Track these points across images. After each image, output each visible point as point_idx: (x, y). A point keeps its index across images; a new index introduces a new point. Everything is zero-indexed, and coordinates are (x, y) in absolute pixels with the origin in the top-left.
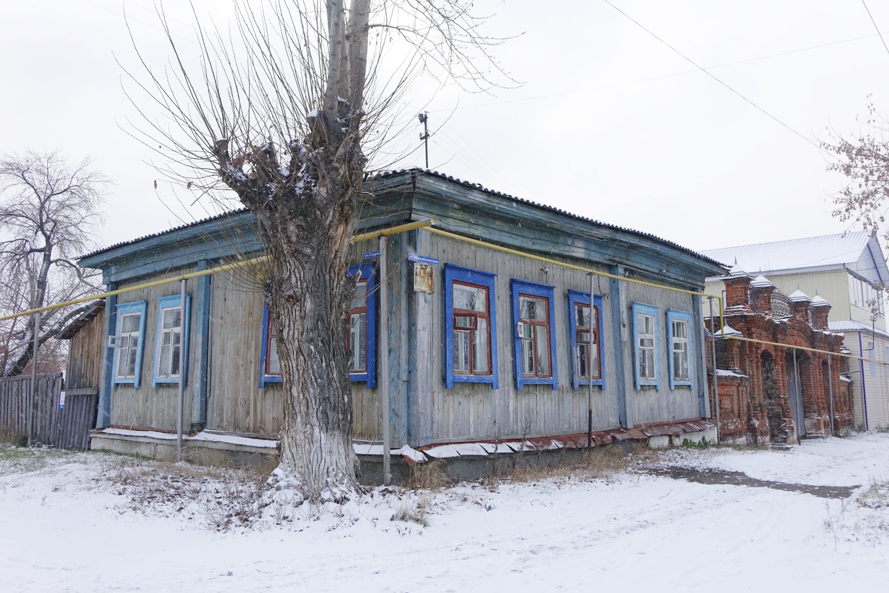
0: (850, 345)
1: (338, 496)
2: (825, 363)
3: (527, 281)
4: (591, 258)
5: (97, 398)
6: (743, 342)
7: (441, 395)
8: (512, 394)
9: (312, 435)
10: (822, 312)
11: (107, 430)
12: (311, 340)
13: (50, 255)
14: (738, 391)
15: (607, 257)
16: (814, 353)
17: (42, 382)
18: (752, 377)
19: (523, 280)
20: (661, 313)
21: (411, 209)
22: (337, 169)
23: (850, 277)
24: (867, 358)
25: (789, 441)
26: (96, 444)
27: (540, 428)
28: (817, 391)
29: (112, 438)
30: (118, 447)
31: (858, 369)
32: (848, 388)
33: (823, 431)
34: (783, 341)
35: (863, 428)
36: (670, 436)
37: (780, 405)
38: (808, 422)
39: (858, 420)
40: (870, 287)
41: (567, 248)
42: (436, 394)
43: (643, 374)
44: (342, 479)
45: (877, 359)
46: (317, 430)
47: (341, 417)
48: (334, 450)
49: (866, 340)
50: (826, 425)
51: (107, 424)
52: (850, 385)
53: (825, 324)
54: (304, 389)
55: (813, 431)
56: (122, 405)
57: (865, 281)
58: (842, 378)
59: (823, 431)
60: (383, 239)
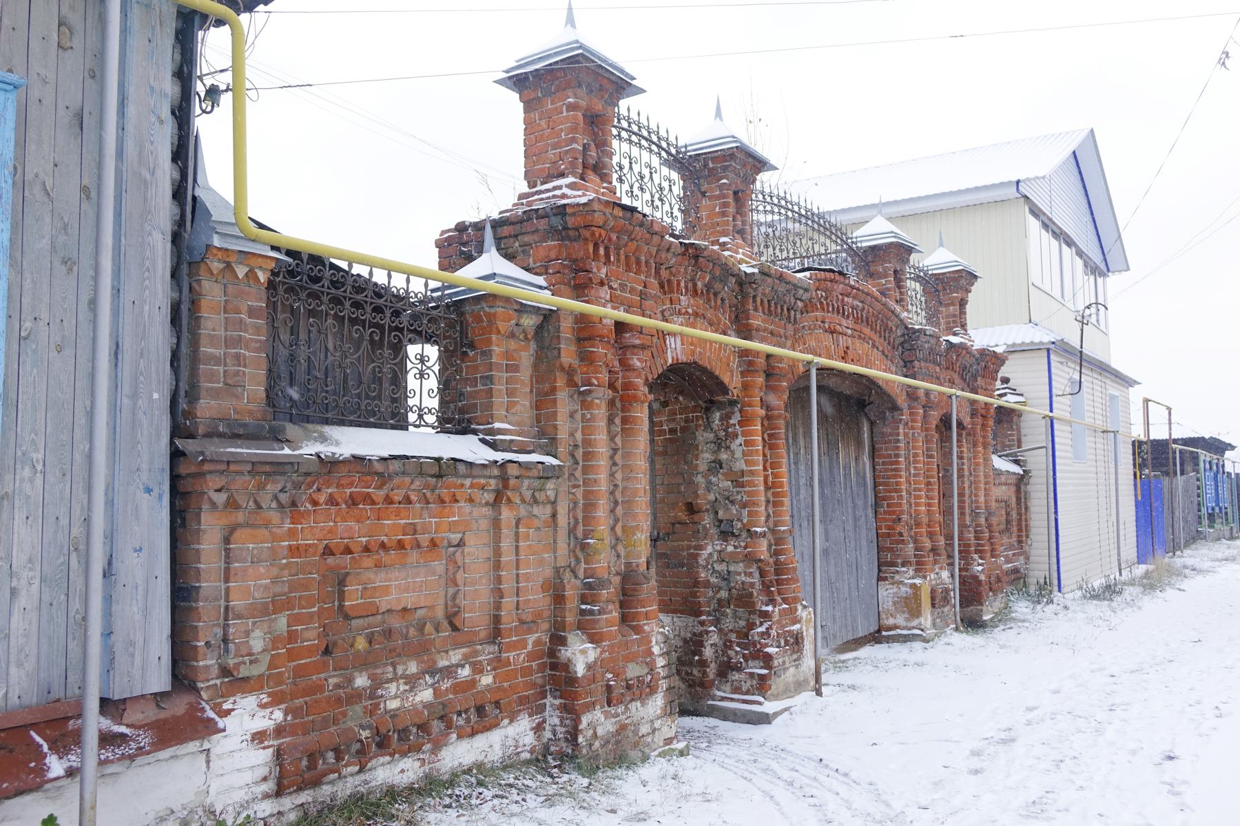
0: (1024, 384)
2: (945, 422)
6: (548, 317)
10: (951, 289)
14: (496, 524)
16: (912, 394)
18: (583, 456)
23: (1034, 224)
24: (1067, 416)
25: (776, 684)
28: (915, 498)
31: (1042, 439)
32: (1018, 491)
33: (926, 619)
34: (773, 337)
35: (1045, 592)
37: (750, 559)
38: (887, 593)
39: (1038, 570)
40: (1079, 263)
45: (1088, 420)
49: (1064, 373)
50: (938, 599)
52: (1021, 481)
53: (959, 322)
55: (900, 620)
57: (1070, 243)
58: (1000, 463)
59: (926, 619)
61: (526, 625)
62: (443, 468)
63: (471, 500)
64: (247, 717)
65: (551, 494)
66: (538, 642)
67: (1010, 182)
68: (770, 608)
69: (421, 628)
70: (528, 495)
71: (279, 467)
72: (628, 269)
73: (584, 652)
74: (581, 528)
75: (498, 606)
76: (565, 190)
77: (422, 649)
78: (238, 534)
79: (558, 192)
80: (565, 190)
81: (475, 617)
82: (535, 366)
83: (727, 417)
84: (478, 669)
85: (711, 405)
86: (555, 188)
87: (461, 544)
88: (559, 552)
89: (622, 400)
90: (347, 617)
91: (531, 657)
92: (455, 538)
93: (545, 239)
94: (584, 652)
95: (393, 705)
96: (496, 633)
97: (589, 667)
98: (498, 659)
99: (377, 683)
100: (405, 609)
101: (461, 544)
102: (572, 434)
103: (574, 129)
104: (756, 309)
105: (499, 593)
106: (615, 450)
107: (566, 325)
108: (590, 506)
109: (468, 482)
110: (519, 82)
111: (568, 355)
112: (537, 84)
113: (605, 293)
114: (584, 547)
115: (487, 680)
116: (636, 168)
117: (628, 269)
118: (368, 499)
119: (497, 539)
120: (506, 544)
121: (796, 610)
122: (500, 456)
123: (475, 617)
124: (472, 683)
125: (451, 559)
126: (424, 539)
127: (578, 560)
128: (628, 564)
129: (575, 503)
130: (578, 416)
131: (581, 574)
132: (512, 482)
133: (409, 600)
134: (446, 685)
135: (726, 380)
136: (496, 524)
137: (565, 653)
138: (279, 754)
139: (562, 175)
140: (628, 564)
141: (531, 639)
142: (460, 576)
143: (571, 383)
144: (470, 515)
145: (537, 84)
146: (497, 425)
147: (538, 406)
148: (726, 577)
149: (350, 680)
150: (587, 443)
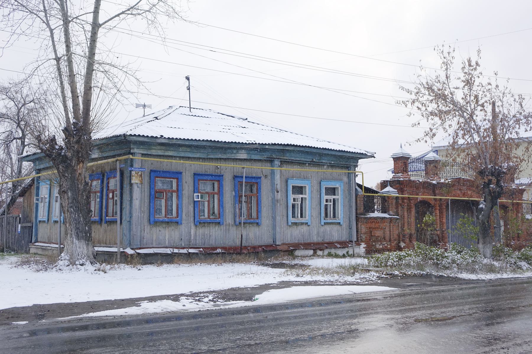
1: (81, 263)
3: (206, 173)
4: (252, 158)
5: (32, 226)
7: (149, 227)
8: (193, 227)
9: (73, 241)
11: (37, 244)
12: (71, 207)
13: (24, 142)
14: (390, 225)
15: (266, 156)
17: (11, 219)
18: (403, 217)
19: (204, 173)
20: (315, 182)
21: (130, 148)
22: (74, 147)
26: (32, 251)
27: (212, 243)
29: (37, 248)
30: (40, 252)
36: (314, 250)
41: (233, 155)
42: (146, 227)
43: (293, 216)
44: (84, 257)
46: (74, 239)
47: (84, 235)
48: (81, 247)
51: (37, 241)
54: (70, 224)
56: (43, 231)
60: (118, 162)
61: (395, 240)
64: (363, 245)
77: (380, 241)
81: (387, 238)
84: (388, 245)
85: (429, 207)
89: (409, 210)
96: (390, 241)
112: (397, 159)
113: (406, 192)
120: (391, 229)
123: (387, 238)
133: (379, 235)
136: (390, 225)
145: (397, 159)
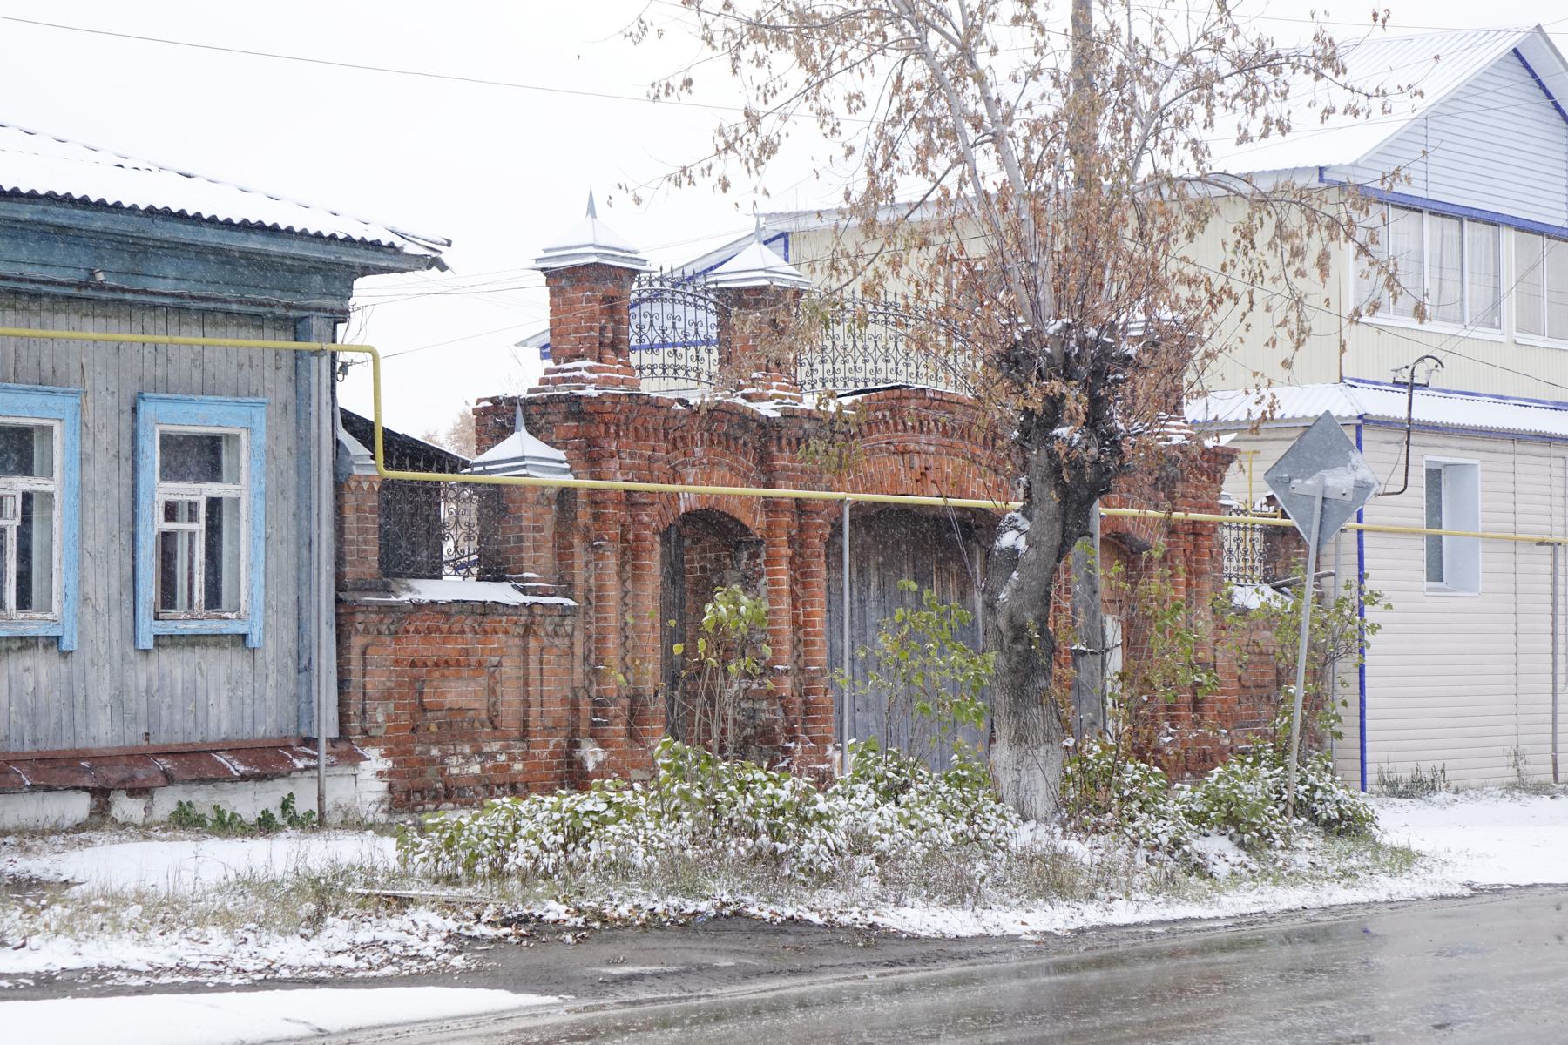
14: (525, 651)
18: (594, 599)
62: (488, 609)
63: (506, 633)
64: (375, 761)
65: (569, 629)
66: (557, 745)
67: (1306, 169)
68: (792, 745)
69: (472, 722)
70: (550, 629)
71: (391, 608)
72: (637, 438)
73: (594, 753)
74: (593, 656)
75: (526, 714)
76: (583, 373)
77: (472, 738)
78: (370, 650)
79: (577, 374)
80: (583, 373)
81: (509, 718)
82: (558, 524)
83: (756, 555)
84: (512, 758)
86: (575, 369)
87: (499, 665)
88: (575, 676)
89: (631, 554)
90: (424, 710)
91: (553, 755)
92: (495, 660)
93: (566, 419)
94: (594, 753)
95: (455, 771)
96: (525, 733)
97: (598, 765)
98: (527, 753)
99: (445, 755)
100: (460, 709)
101: (499, 665)
102: (586, 581)
103: (592, 318)
104: (781, 450)
105: (527, 704)
106: (626, 594)
107: (582, 499)
108: (601, 640)
109: (504, 619)
110: (552, 275)
111: (584, 515)
112: (567, 280)
113: (614, 464)
114: (596, 671)
115: (518, 767)
116: (657, 323)
117: (637, 438)
118: (438, 629)
119: (526, 663)
120: (533, 665)
121: (825, 749)
122: (529, 599)
123: (509, 718)
124: (509, 767)
125: (492, 675)
126: (473, 659)
127: (591, 682)
128: (636, 690)
129: (590, 637)
130: (592, 567)
131: (593, 694)
132: (538, 619)
133: (463, 703)
134: (489, 765)
135: (747, 522)
136: (525, 651)
137: (578, 753)
138: (391, 787)
139: (580, 357)
140: (636, 690)
141: (552, 742)
142: (498, 689)
143: (586, 538)
144: (503, 648)
145: (567, 280)
146: (526, 575)
147: (560, 557)
148: (753, 714)
149: (429, 751)
150: (600, 588)
